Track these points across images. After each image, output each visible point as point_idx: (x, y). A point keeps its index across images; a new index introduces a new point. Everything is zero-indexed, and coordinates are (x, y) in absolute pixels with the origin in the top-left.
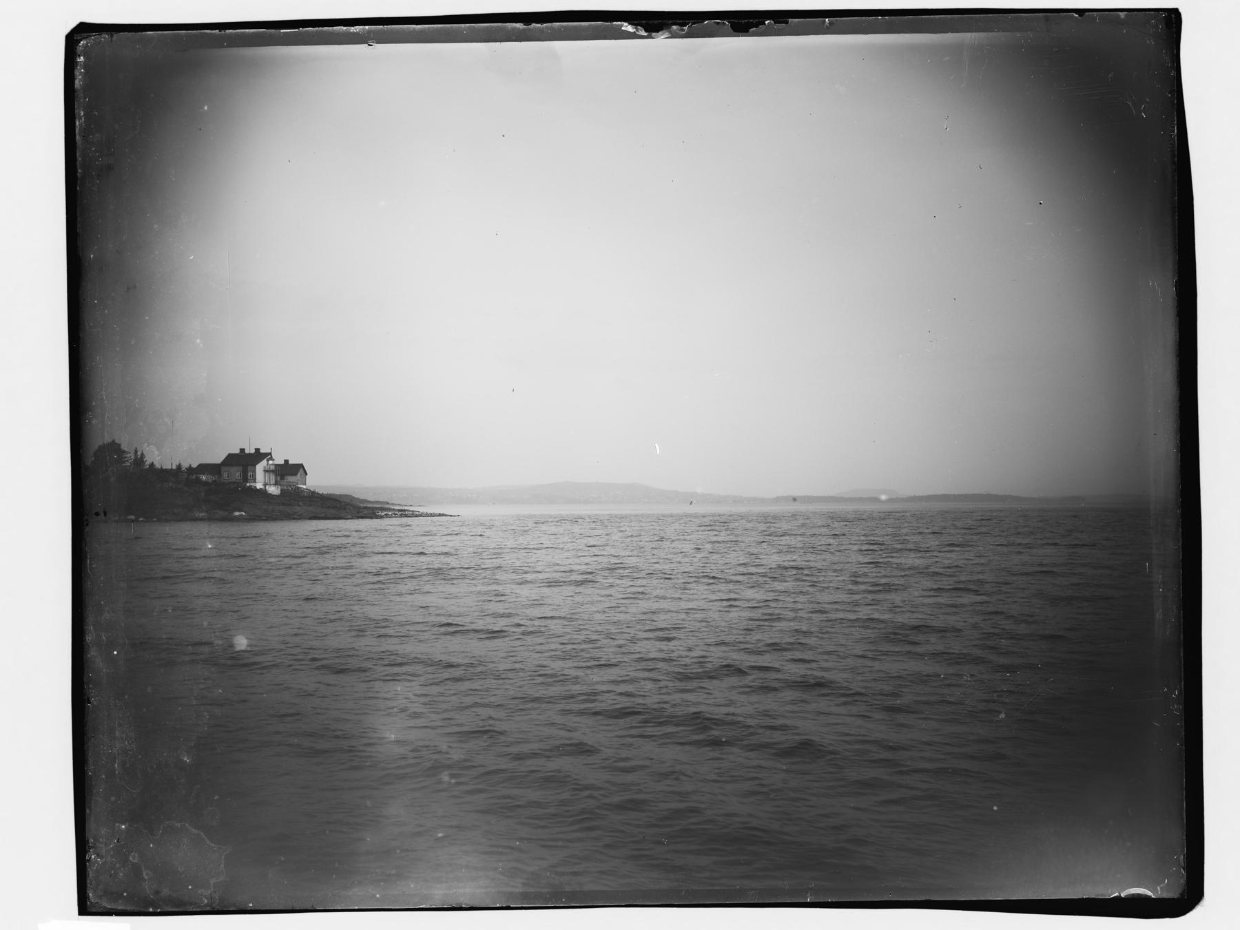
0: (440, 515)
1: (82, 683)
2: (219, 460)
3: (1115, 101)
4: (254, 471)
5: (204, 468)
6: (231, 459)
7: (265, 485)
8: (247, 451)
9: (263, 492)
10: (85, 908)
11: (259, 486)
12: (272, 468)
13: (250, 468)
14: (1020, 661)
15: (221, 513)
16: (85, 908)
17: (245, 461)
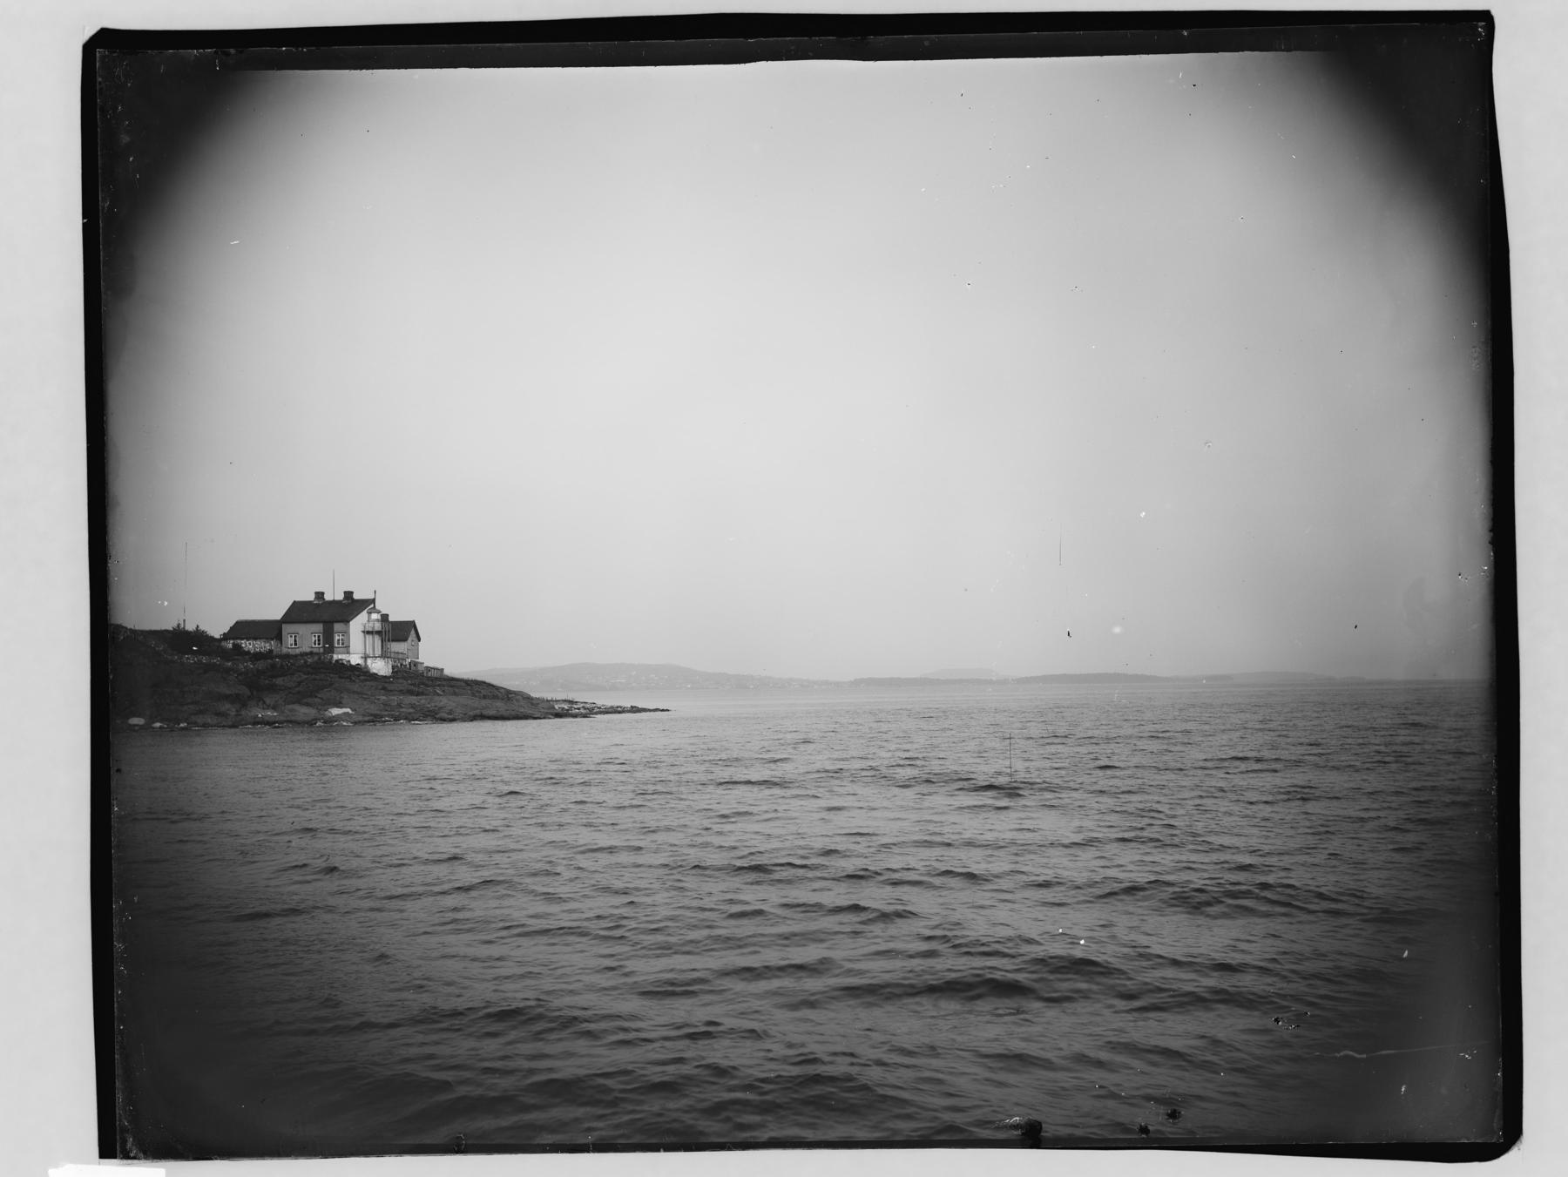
0: (634, 710)
1: (1424, 1145)
2: (277, 615)
3: (1420, 103)
4: (346, 633)
5: (243, 629)
6: (299, 613)
7: (366, 657)
8: (328, 597)
9: (360, 672)
10: (109, 1148)
11: (355, 659)
12: (378, 626)
13: (337, 627)
14: (1339, 907)
15: (303, 712)
16: (109, 1148)
17: (330, 613)
